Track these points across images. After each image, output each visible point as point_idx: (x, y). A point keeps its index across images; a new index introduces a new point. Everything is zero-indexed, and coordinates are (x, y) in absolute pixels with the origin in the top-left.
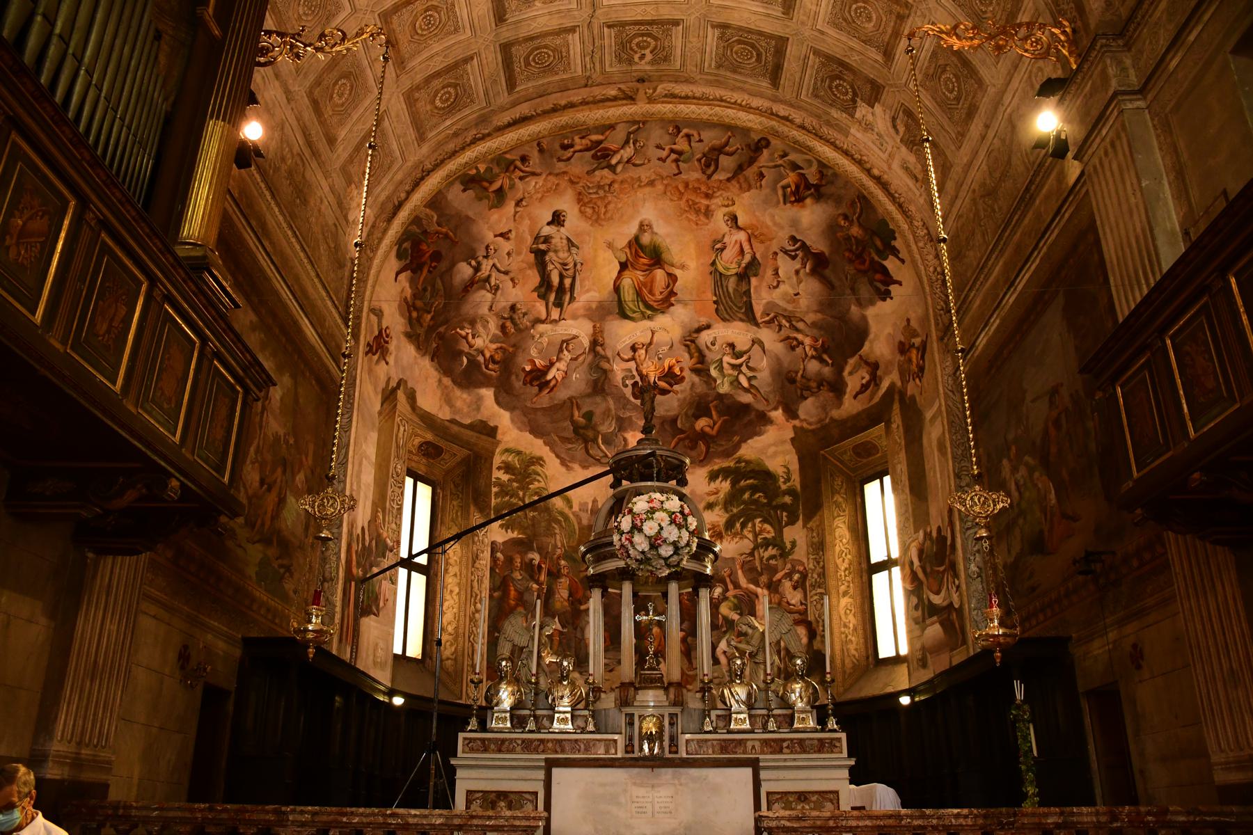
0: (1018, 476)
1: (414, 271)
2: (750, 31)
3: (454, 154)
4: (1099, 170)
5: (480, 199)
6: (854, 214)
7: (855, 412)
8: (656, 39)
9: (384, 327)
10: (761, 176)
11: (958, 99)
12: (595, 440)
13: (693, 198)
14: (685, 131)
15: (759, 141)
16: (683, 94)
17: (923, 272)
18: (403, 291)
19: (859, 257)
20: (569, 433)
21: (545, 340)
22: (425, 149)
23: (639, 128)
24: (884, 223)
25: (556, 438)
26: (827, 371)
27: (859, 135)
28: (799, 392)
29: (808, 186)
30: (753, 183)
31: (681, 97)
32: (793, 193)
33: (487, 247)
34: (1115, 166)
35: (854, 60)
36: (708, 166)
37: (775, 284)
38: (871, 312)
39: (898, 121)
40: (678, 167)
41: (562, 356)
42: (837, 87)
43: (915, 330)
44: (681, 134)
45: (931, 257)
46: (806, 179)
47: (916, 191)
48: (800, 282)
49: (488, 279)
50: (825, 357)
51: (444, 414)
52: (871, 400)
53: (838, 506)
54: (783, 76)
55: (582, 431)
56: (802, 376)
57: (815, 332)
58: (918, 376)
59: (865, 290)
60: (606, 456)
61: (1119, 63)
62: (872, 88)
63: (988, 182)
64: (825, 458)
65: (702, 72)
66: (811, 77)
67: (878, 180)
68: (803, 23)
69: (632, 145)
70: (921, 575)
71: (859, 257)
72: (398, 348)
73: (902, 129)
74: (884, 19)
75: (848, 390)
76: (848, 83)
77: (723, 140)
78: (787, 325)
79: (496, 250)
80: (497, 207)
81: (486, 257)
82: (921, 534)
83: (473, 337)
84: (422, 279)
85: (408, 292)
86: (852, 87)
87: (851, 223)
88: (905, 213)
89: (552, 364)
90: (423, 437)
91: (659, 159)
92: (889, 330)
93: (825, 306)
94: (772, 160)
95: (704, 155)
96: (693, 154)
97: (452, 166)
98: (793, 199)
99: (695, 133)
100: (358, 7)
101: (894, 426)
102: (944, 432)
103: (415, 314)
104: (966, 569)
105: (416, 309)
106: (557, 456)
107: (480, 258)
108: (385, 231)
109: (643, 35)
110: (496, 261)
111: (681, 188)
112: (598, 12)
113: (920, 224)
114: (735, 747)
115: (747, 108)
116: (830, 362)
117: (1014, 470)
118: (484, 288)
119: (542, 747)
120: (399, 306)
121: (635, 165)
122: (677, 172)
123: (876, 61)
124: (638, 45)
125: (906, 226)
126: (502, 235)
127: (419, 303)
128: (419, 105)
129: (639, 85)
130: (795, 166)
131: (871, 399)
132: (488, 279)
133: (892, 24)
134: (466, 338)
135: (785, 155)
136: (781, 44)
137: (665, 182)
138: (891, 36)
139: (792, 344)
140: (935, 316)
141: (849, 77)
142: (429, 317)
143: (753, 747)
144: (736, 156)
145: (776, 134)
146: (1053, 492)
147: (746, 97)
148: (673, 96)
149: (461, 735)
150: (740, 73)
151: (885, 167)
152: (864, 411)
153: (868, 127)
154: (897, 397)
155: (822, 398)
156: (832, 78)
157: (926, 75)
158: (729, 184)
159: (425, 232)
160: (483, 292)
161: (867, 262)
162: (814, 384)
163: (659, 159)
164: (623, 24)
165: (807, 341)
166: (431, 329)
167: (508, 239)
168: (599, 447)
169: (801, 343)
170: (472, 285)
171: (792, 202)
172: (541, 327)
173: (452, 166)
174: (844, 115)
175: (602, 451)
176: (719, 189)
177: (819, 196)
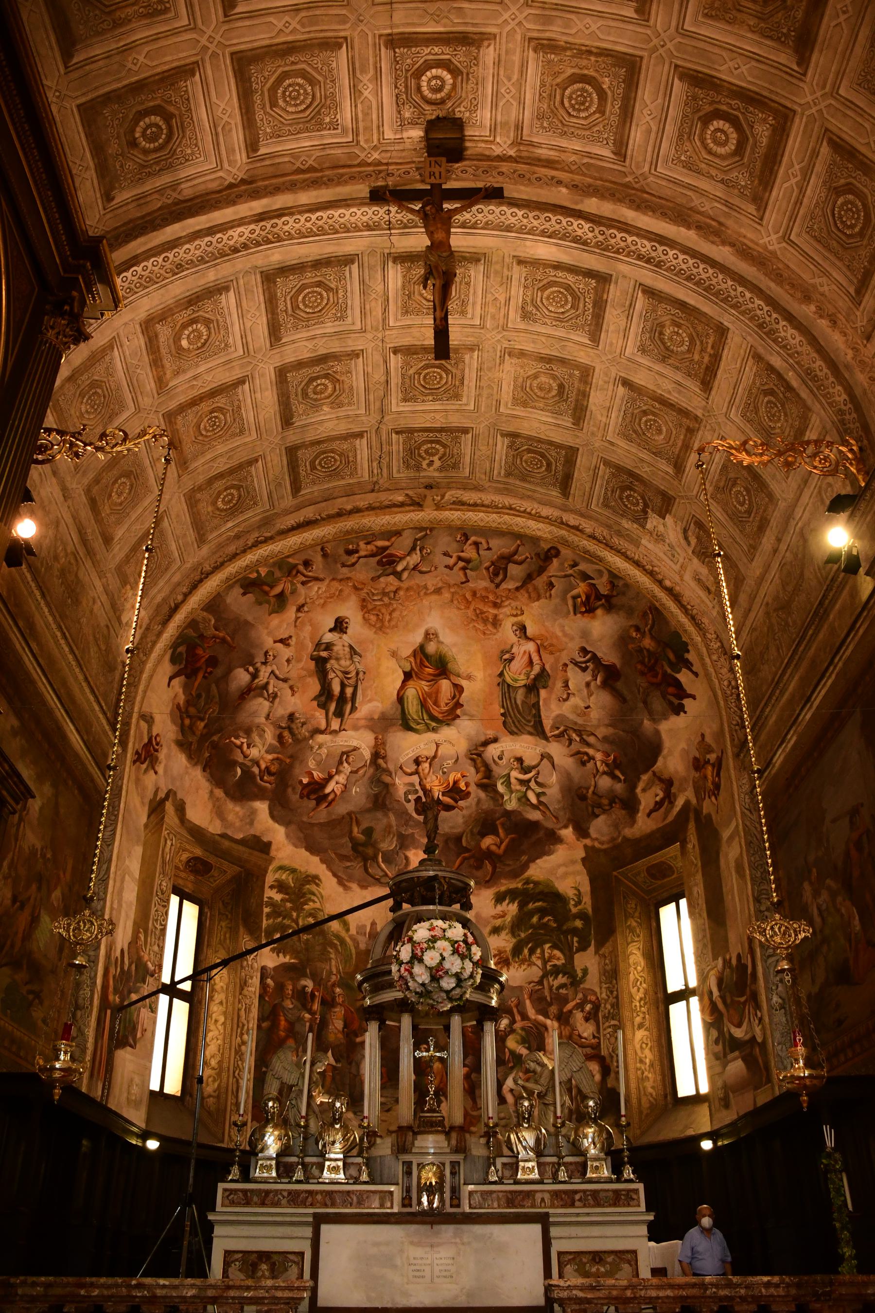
1: (187, 677)
2: (540, 441)
3: (234, 556)
5: (260, 604)
8: (444, 446)
9: (154, 734)
10: (551, 585)
11: (749, 512)
12: (375, 858)
15: (549, 550)
16: (472, 502)
17: (717, 686)
18: (176, 696)
20: (347, 850)
21: (324, 751)
22: (205, 550)
24: (677, 635)
25: (333, 856)
26: (619, 787)
28: (590, 809)
29: (599, 596)
30: (542, 591)
31: (469, 505)
32: (584, 604)
33: (266, 653)
35: (644, 471)
36: (496, 574)
37: (565, 697)
39: (690, 533)
40: (465, 574)
41: (341, 768)
42: (628, 497)
44: (469, 542)
45: (724, 671)
48: (590, 694)
49: (265, 686)
50: (617, 773)
51: (215, 828)
52: (664, 819)
53: (632, 930)
55: (361, 849)
56: (593, 793)
57: (606, 747)
58: (714, 794)
59: (658, 704)
60: (386, 875)
67: (670, 591)
68: (593, 434)
70: (721, 1006)
72: (168, 757)
73: (693, 541)
75: (641, 808)
78: (578, 739)
79: (275, 657)
80: (277, 612)
81: (265, 663)
82: (720, 961)
83: (249, 747)
84: (197, 684)
85: (182, 699)
86: (643, 498)
87: (643, 635)
88: (698, 625)
89: (331, 777)
90: (192, 852)
92: (683, 745)
95: (493, 563)
97: (231, 569)
99: (483, 541)
100: (142, 406)
103: (187, 722)
104: (769, 1000)
105: (189, 716)
106: (335, 875)
107: (259, 665)
108: (159, 634)
109: (432, 442)
110: (274, 667)
111: (469, 596)
112: (386, 419)
113: (714, 636)
114: (523, 1200)
115: (537, 517)
117: (816, 894)
118: (262, 696)
119: (310, 1199)
120: (172, 714)
121: (421, 572)
123: (667, 473)
124: (426, 451)
126: (281, 641)
127: (192, 710)
128: (201, 505)
129: (427, 492)
130: (585, 576)
132: (265, 686)
133: (682, 437)
134: (240, 747)
135: (575, 565)
136: (571, 454)
137: (452, 590)
139: (583, 759)
140: (730, 731)
141: (639, 487)
142: (202, 724)
143: (543, 1200)
144: (524, 565)
147: (536, 505)
148: (460, 504)
149: (221, 1186)
150: (530, 482)
151: (677, 578)
152: (658, 830)
153: (659, 538)
154: (692, 815)
158: (518, 594)
159: (201, 636)
160: (261, 700)
161: (660, 676)
162: (605, 801)
164: (411, 431)
165: (599, 756)
166: (204, 738)
167: (288, 645)
168: (379, 866)
170: (248, 692)
171: (582, 613)
172: (321, 738)
173: (231, 569)
174: (635, 526)
175: (383, 870)
176: (508, 598)
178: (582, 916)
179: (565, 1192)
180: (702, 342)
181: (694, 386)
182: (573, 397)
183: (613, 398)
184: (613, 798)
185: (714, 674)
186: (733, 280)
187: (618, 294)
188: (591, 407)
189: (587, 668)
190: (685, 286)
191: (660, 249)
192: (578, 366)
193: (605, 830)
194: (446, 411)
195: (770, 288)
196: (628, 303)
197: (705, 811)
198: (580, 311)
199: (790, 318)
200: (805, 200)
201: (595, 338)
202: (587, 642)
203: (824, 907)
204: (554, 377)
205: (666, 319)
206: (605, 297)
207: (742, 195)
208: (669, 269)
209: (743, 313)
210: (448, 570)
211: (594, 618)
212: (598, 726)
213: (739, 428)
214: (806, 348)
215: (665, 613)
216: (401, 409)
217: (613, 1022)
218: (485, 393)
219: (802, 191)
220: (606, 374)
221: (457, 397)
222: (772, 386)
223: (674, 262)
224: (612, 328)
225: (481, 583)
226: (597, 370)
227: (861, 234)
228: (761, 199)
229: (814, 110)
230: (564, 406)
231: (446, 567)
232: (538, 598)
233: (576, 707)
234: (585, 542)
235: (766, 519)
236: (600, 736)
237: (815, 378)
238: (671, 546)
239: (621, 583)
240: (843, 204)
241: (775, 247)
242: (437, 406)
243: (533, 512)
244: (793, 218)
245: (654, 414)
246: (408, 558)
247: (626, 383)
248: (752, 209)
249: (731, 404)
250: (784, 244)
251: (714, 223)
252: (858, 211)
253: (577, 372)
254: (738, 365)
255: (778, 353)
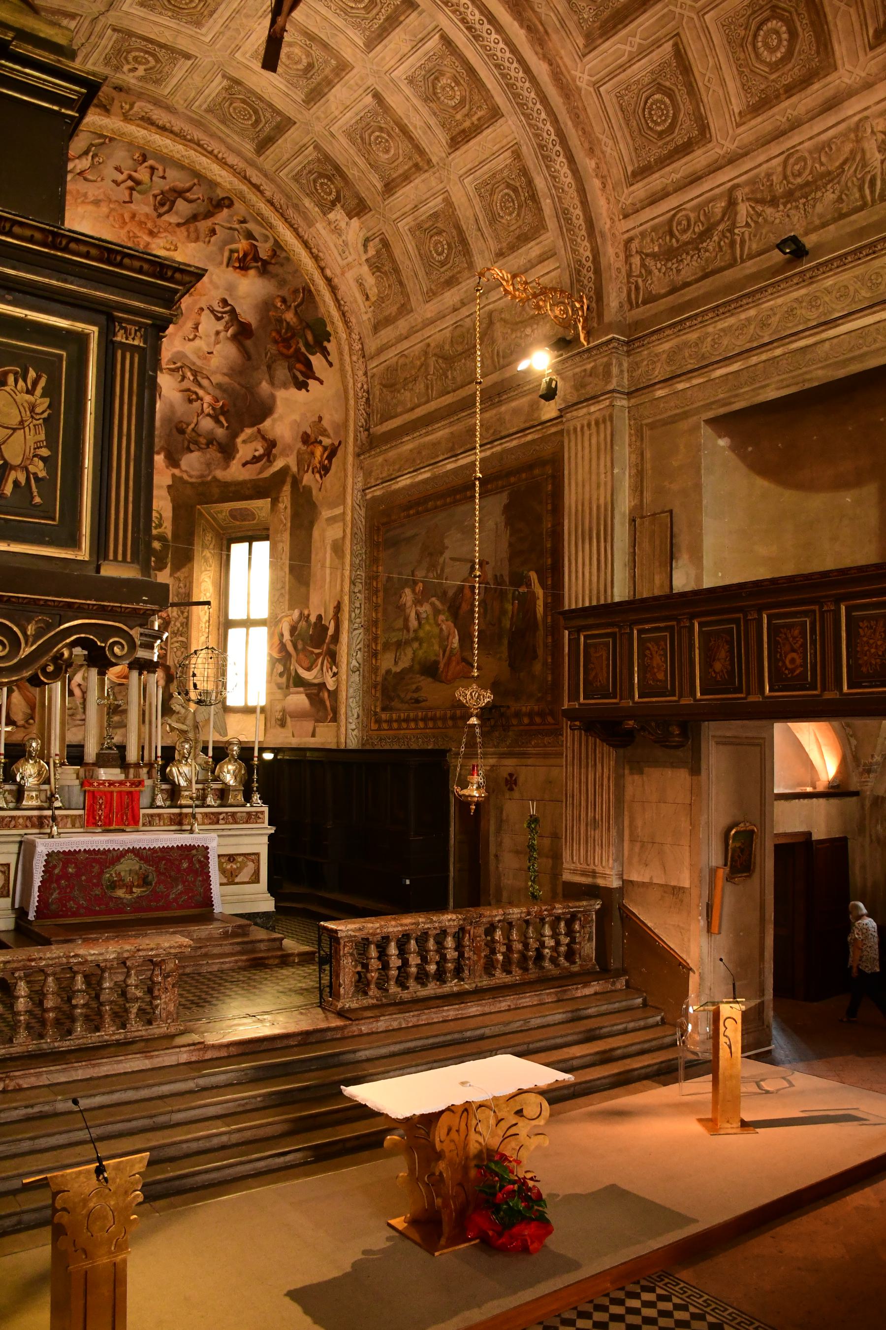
0: (421, 609)
2: (261, 99)
4: (579, 433)
6: (294, 301)
7: (241, 478)
8: (157, 60)
10: (213, 232)
11: (443, 264)
13: (136, 231)
14: (151, 162)
15: (223, 199)
16: (161, 123)
17: (351, 385)
19: (286, 342)
23: (104, 143)
24: (321, 323)
26: (220, 432)
27: (323, 232)
28: (186, 443)
29: (256, 258)
30: (202, 235)
31: (158, 127)
32: (239, 260)
34: (594, 441)
35: (352, 173)
36: (162, 204)
37: (191, 337)
38: (282, 395)
39: (371, 244)
40: (131, 195)
42: (322, 184)
43: (325, 430)
44: (146, 164)
45: (360, 373)
46: (256, 251)
47: (362, 306)
48: (217, 342)
50: (222, 419)
52: (260, 473)
53: (206, 560)
54: (272, 149)
56: (193, 430)
57: (218, 393)
58: (319, 472)
59: (282, 372)
61: (620, 365)
62: (358, 205)
63: (447, 347)
64: (201, 513)
65: (189, 106)
66: (301, 163)
67: (329, 280)
68: (318, 118)
69: (90, 158)
70: (290, 648)
71: (286, 342)
73: (372, 252)
74: (401, 159)
75: (238, 456)
76: (336, 187)
77: (188, 185)
78: (192, 378)
82: (296, 613)
86: (338, 192)
87: (288, 308)
88: (346, 323)
91: (114, 181)
92: (296, 417)
93: (235, 372)
94: (229, 222)
95: (162, 193)
96: (151, 187)
98: (237, 265)
99: (161, 168)
101: (281, 506)
102: (344, 537)
104: (348, 663)
109: (146, 52)
111: (127, 217)
112: (111, 13)
113: (357, 337)
115: (223, 163)
116: (226, 425)
117: (418, 602)
119: (13, 823)
121: (86, 179)
122: (127, 199)
123: (374, 186)
124: (135, 59)
125: (344, 336)
129: (115, 94)
130: (250, 236)
131: (261, 471)
133: (406, 167)
135: (244, 221)
136: (285, 124)
137: (112, 206)
138: (400, 176)
139: (191, 398)
140: (356, 431)
141: (338, 181)
144: (194, 205)
145: (243, 198)
146: (457, 637)
147: (223, 149)
148: (148, 121)
150: (228, 126)
151: (338, 271)
152: (251, 481)
153: (336, 231)
154: (289, 480)
155: (208, 456)
156: (321, 175)
157: (419, 226)
158: (177, 229)
161: (292, 350)
162: (203, 441)
163: (114, 181)
164: (130, 34)
165: (208, 399)
169: (199, 398)
171: (235, 268)
174: (317, 209)
176: (166, 230)
177: (264, 269)
178: (161, 538)
179: (213, 813)
180: (471, 109)
181: (443, 137)
182: (316, 79)
183: (357, 101)
184: (211, 441)
185: (350, 372)
186: (537, 95)
187: (416, 23)
188: (331, 96)
189: (222, 318)
190: (490, 70)
191: (487, 26)
192: (337, 56)
193: (197, 465)
194: (179, 32)
195: (566, 125)
196: (420, 36)
197: (305, 482)
198: (370, 16)
199: (571, 160)
200: (629, 71)
201: (370, 45)
202: (231, 295)
203: (424, 615)
204: (308, 55)
205: (449, 72)
206: (402, 18)
207: (579, 25)
208: (484, 47)
209: (530, 125)
210: (114, 185)
211: (244, 276)
212: (214, 373)
213: (467, 195)
214: (572, 192)
215: (317, 298)
216: (131, 11)
217: (181, 639)
218: (229, 34)
219: (630, 62)
220: (362, 79)
221: (198, 24)
222: (518, 184)
223: (492, 45)
224: (392, 46)
225: (143, 207)
226: (355, 71)
227: (661, 135)
228: (594, 40)
229: (678, 10)
230: (303, 82)
231: (113, 181)
232: (197, 239)
233: (199, 349)
234: (263, 205)
235: (457, 279)
236: (214, 382)
237: (569, 220)
238: (345, 243)
239: (283, 255)
240: (657, 101)
241: (583, 85)
242: (172, 24)
243: (220, 156)
244: (611, 75)
245: (389, 135)
246: (77, 161)
247: (377, 96)
248: (581, 41)
249: (470, 172)
250: (591, 89)
251: (540, 27)
252: (667, 116)
253: (333, 62)
254: (495, 148)
255: (546, 179)
